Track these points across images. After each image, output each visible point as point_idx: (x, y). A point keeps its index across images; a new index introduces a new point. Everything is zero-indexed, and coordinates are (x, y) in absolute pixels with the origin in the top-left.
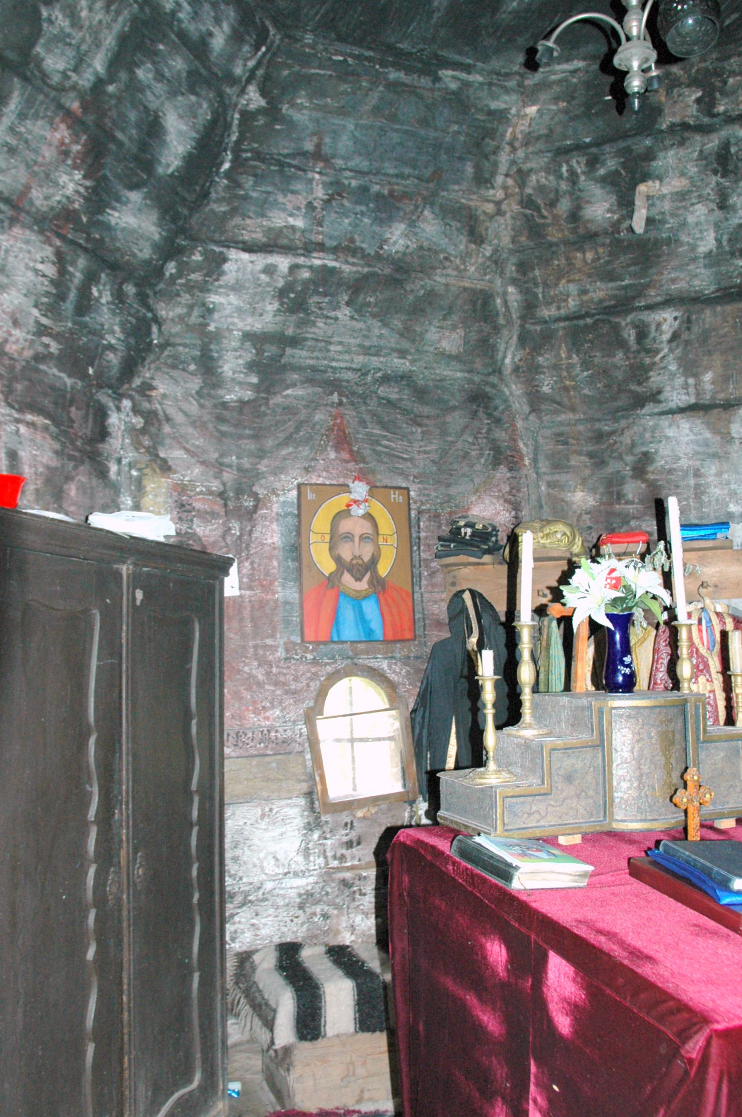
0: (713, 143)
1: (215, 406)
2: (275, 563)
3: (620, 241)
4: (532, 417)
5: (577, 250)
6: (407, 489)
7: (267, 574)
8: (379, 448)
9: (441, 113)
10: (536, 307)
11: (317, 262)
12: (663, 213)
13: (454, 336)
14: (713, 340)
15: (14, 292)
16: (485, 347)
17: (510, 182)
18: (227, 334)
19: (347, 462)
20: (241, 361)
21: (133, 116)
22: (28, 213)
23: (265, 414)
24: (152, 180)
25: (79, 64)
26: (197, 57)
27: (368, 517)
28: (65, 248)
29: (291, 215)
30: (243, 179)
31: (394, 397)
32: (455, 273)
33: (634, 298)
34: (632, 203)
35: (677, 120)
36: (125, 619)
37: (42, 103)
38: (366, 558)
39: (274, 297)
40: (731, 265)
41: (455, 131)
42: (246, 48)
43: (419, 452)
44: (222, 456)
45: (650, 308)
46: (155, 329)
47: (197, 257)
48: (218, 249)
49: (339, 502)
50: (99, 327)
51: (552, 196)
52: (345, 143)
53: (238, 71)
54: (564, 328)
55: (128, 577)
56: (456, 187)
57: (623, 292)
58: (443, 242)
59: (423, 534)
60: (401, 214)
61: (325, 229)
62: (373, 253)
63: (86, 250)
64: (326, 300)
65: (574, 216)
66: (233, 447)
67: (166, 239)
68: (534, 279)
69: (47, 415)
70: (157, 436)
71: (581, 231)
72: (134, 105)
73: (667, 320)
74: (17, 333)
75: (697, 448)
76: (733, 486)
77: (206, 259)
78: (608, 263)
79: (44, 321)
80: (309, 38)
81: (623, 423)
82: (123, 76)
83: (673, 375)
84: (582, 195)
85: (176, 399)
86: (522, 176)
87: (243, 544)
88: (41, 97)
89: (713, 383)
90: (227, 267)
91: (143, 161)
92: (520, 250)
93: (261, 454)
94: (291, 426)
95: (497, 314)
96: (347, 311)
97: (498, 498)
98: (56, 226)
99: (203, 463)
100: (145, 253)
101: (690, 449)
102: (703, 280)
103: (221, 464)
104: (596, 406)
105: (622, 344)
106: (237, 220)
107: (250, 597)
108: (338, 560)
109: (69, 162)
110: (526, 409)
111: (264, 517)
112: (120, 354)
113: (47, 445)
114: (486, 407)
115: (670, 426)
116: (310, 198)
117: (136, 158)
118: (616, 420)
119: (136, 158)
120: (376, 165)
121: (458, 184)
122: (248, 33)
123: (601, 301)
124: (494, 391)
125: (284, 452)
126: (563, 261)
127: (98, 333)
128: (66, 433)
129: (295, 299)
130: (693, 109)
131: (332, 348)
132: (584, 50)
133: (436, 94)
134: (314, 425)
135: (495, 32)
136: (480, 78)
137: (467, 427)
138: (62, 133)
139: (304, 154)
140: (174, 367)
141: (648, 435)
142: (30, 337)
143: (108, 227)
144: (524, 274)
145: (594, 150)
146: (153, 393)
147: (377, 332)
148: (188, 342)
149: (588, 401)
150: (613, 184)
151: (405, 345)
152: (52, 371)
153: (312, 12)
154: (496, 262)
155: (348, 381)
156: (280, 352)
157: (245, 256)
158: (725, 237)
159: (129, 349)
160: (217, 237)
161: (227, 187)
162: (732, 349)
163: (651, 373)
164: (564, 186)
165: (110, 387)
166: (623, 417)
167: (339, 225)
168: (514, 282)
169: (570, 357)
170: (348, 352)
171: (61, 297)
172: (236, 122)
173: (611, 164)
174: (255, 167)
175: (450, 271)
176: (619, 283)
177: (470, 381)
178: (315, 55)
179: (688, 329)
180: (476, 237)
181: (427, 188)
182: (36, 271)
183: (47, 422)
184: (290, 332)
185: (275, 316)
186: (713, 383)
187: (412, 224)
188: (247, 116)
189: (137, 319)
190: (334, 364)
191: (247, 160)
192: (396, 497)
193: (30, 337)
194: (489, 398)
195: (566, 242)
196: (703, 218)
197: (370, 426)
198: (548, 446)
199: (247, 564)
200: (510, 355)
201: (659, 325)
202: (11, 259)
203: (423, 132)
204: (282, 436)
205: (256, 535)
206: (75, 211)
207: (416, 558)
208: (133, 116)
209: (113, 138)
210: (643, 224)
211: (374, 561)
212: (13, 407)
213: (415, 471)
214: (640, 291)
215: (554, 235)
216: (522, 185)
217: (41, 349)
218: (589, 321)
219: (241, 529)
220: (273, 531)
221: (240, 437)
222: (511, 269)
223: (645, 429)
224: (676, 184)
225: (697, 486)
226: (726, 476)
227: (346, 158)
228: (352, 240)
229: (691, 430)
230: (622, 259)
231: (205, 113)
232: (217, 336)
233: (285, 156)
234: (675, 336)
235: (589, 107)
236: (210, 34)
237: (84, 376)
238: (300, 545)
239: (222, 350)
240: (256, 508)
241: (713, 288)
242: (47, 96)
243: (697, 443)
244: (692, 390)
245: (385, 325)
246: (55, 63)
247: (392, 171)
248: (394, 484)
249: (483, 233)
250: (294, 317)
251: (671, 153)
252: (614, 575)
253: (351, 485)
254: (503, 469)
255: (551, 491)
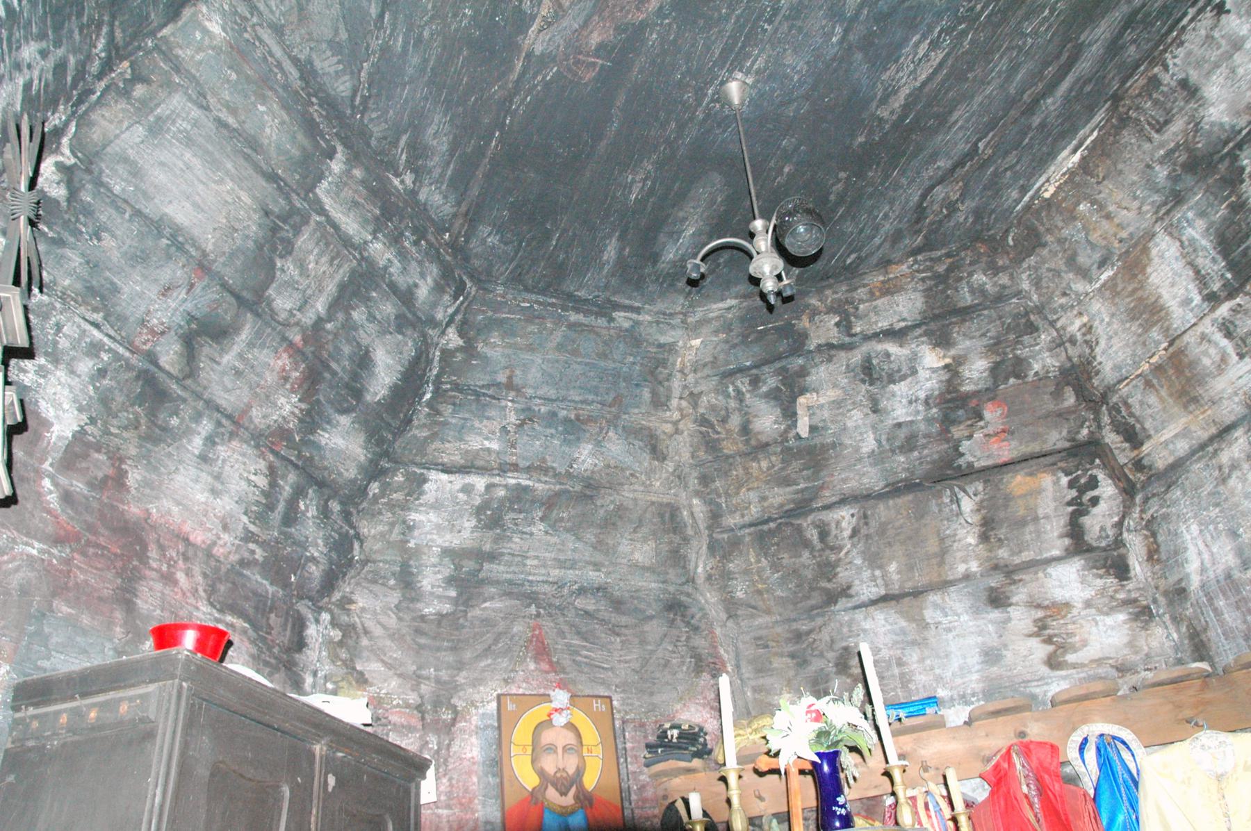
0: (856, 357)
1: (413, 619)
2: (475, 779)
3: (790, 449)
4: (730, 624)
5: (754, 459)
6: (610, 697)
7: (466, 791)
8: (579, 658)
9: (618, 348)
10: (721, 516)
11: (513, 481)
12: (824, 421)
13: (646, 548)
14: (891, 532)
15: (226, 498)
16: (676, 557)
17: (684, 403)
18: (426, 550)
19: (547, 672)
20: (440, 576)
21: (347, 350)
22: (247, 429)
23: (463, 627)
24: (360, 406)
25: (304, 305)
26: (403, 303)
27: (571, 726)
28: (277, 463)
29: (487, 439)
30: (441, 407)
31: (591, 608)
32: (642, 488)
33: (811, 500)
34: (795, 414)
35: (822, 341)
36: (315, 802)
37: (269, 335)
38: (571, 770)
39: (471, 514)
40: (894, 461)
41: (630, 362)
42: (447, 297)
43: (620, 661)
44: (420, 668)
45: (827, 507)
46: (356, 546)
47: (399, 478)
48: (418, 471)
49: (539, 713)
50: (303, 539)
51: (723, 413)
52: (534, 375)
53: (439, 316)
54: (750, 534)
55: (321, 757)
56: (636, 411)
57: (800, 496)
58: (628, 460)
59: (629, 745)
60: (588, 435)
61: (518, 451)
62: (563, 472)
63: (296, 466)
64: (522, 516)
65: (745, 429)
66: (431, 659)
67: (371, 461)
68: (716, 490)
69: (246, 618)
70: (355, 648)
71: (753, 442)
72: (348, 341)
73: (845, 518)
74: (225, 537)
75: (895, 637)
76: (937, 671)
77: (407, 479)
78: (782, 469)
79: (252, 528)
80: (500, 290)
81: (819, 621)
82: (341, 316)
83: (859, 569)
84: (750, 410)
85: (375, 613)
86: (694, 398)
87: (443, 755)
88: (269, 330)
89: (899, 573)
90: (426, 486)
91: (354, 390)
92: (701, 464)
93: (460, 666)
94: (489, 637)
95: (686, 526)
96: (542, 526)
97: (704, 705)
98: (273, 443)
99: (400, 675)
100: (351, 472)
101: (888, 639)
102: (872, 479)
103: (419, 677)
104: (791, 607)
105: (807, 544)
106: (437, 444)
107: (448, 816)
108: (541, 773)
109: (288, 386)
110: (724, 616)
111: (463, 731)
112: (322, 567)
113: (244, 649)
114: (683, 616)
115: (865, 618)
116: (504, 423)
117: (347, 386)
118: (812, 619)
119: (347, 386)
120: (563, 393)
121: (638, 407)
122: (448, 285)
123: (782, 505)
124: (690, 600)
125: (482, 664)
126: (741, 471)
127: (303, 545)
128: (264, 639)
129: (491, 516)
130: (835, 331)
131: (529, 562)
132: (734, 290)
133: (612, 332)
134: (513, 636)
135: (657, 279)
136: (648, 318)
137: (665, 636)
138: (284, 361)
139: (498, 385)
140: (375, 582)
141: (845, 630)
142: (237, 542)
143: (318, 447)
144: (706, 486)
145: (754, 371)
146: (353, 607)
147: (571, 546)
148: (388, 558)
149: (782, 601)
150: (775, 398)
151: (598, 557)
152: (256, 578)
153: (502, 269)
154: (680, 477)
155: (545, 594)
156: (477, 567)
157: (444, 477)
158: (884, 437)
159: (331, 562)
160: (418, 459)
161: (429, 414)
162: (910, 538)
163: (839, 569)
164: (733, 404)
165: (310, 599)
166: (818, 614)
167: (531, 447)
168: (697, 494)
169: (759, 561)
170: (544, 566)
171: (271, 507)
172: (437, 358)
173: (771, 382)
174: (454, 397)
175: (636, 487)
176: (795, 487)
177: (665, 591)
178: (506, 303)
179: (866, 524)
180: (656, 451)
181: (609, 412)
182: (249, 481)
183: (246, 625)
184: (487, 547)
185: (472, 532)
186: (899, 573)
187: (598, 444)
188: (447, 354)
189: (340, 534)
190: (530, 578)
191: (446, 391)
192: (598, 705)
193: (237, 542)
194: (686, 607)
195: (744, 455)
196: (860, 422)
197: (568, 636)
198: (749, 651)
199: (445, 780)
200: (701, 565)
201: (838, 523)
202: (227, 468)
203: (602, 364)
204: (480, 647)
205: (454, 749)
206: (289, 431)
207: (623, 771)
208: (347, 350)
209: (328, 367)
210: (807, 429)
211: (580, 772)
212: (214, 607)
213: (617, 681)
214: (815, 493)
215: (729, 448)
216: (695, 406)
217: (246, 555)
218: (772, 525)
219: (439, 744)
220: (472, 744)
221: (438, 649)
222: (693, 482)
223: (841, 625)
224: (830, 394)
225: (902, 675)
226: (928, 662)
227: (536, 388)
228: (544, 460)
229: (886, 619)
230: (794, 463)
231: (410, 350)
232: (417, 552)
233: (483, 387)
234: (855, 532)
235: (745, 337)
236: (416, 286)
237: (286, 585)
238: (501, 758)
239: (421, 565)
240: (454, 721)
241: (882, 484)
242: (274, 329)
243: (894, 632)
244: (880, 581)
245: (579, 539)
246: (283, 303)
247: (577, 398)
248: (596, 693)
249: (665, 451)
250: (491, 533)
251: (822, 368)
252: (813, 708)
253: (551, 693)
254: (706, 676)
255: (757, 696)
